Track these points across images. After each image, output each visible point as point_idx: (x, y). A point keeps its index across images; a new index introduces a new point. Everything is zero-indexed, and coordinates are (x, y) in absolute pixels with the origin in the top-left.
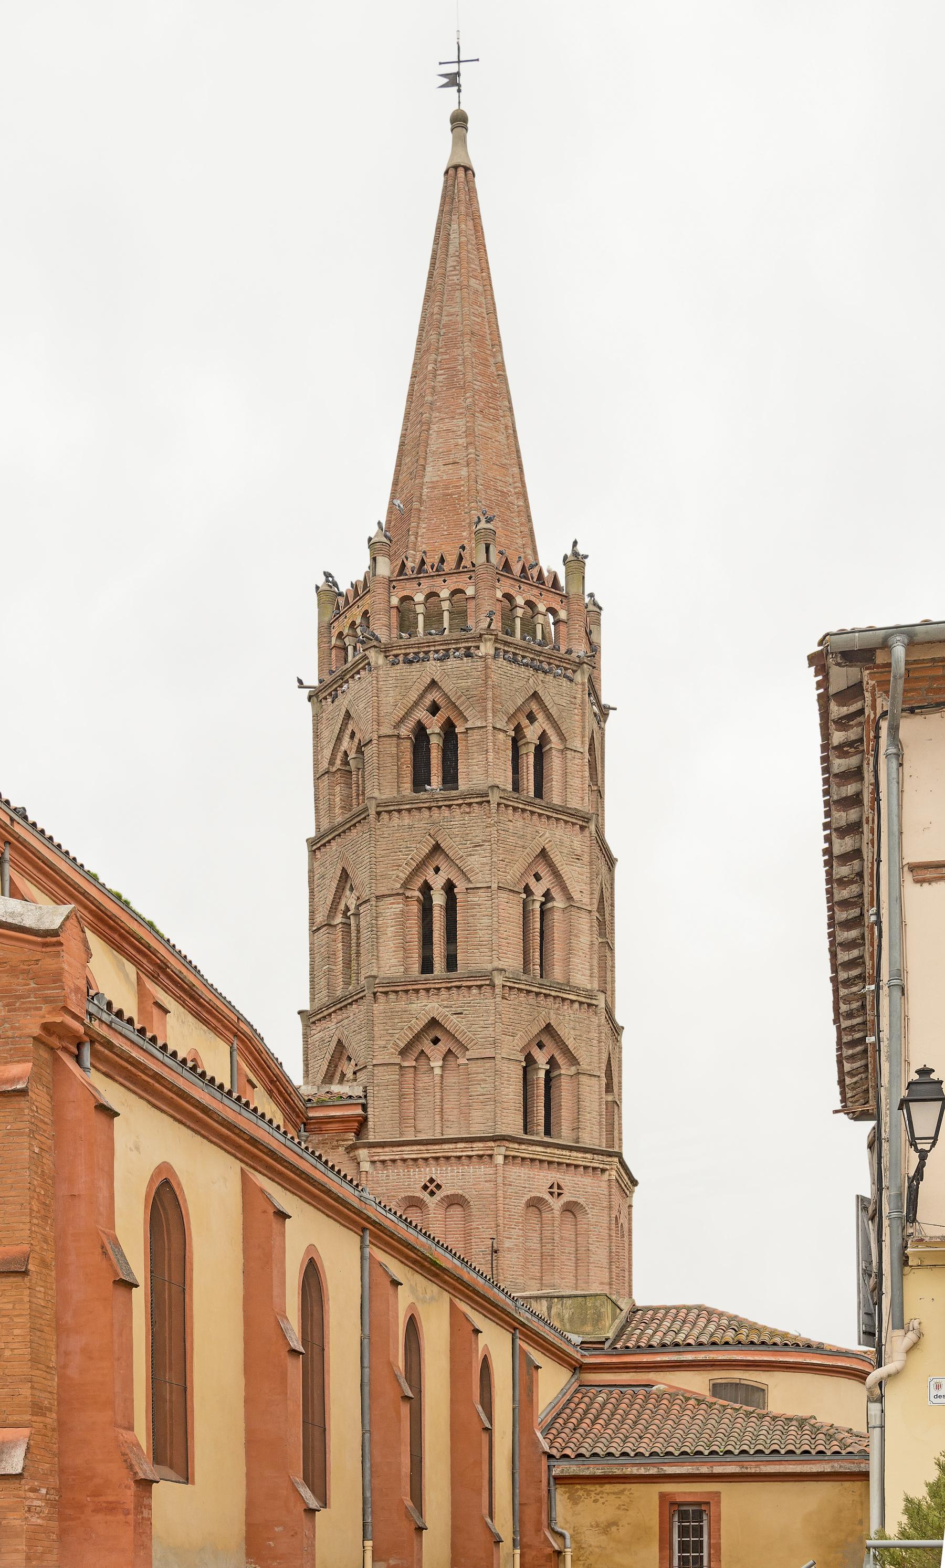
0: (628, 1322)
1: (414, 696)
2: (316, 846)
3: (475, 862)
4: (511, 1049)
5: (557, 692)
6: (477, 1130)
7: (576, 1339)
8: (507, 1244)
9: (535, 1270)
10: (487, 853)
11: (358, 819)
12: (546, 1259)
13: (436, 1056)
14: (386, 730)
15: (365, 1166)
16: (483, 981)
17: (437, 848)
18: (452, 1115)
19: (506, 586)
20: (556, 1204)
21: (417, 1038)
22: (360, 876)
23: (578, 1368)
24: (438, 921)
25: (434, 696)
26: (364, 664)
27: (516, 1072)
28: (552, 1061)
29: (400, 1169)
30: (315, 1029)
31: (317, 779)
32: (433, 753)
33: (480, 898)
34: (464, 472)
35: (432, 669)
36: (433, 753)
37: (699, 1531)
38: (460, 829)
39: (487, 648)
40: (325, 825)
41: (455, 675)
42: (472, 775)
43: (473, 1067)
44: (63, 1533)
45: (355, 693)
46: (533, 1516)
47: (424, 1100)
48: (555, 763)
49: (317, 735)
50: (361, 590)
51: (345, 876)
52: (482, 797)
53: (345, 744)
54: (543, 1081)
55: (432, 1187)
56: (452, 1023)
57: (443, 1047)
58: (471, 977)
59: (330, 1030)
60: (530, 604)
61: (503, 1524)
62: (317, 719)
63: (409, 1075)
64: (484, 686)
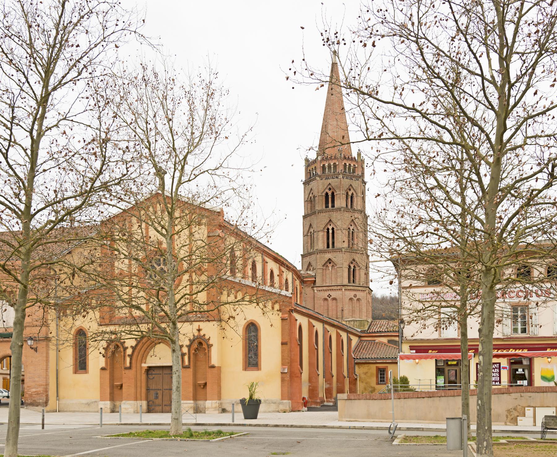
0: (370, 325)
1: (326, 187)
2: (305, 217)
3: (339, 223)
4: (346, 265)
5: (356, 184)
6: (339, 283)
7: (359, 330)
8: (345, 308)
9: (351, 314)
10: (341, 221)
11: (314, 213)
12: (353, 312)
13: (330, 266)
14: (320, 194)
15: (316, 291)
16: (340, 250)
17: (330, 220)
18: (333, 279)
19: (345, 161)
20: (355, 299)
21: (326, 262)
22: (314, 226)
23: (360, 337)
24: (330, 235)
25: (330, 186)
26: (315, 179)
27: (347, 270)
28: (354, 267)
29: (323, 292)
30: (304, 259)
31: (305, 202)
32: (329, 198)
33: (339, 232)
34: (336, 134)
35: (330, 181)
36: (329, 198)
37: (384, 374)
38: (335, 216)
39: (341, 176)
40: (306, 213)
41: (334, 182)
42: (337, 204)
43: (338, 269)
44: (291, 380)
45: (313, 184)
46: (351, 371)
47: (328, 276)
48: (355, 199)
49: (305, 192)
50: (315, 161)
51: (311, 225)
52: (339, 209)
53: (311, 195)
54: (352, 273)
55: (329, 296)
56: (334, 259)
57: (331, 264)
58: (338, 249)
59: (307, 259)
60: (350, 165)
61: (345, 373)
62: (305, 188)
63: (324, 271)
64: (341, 183)
